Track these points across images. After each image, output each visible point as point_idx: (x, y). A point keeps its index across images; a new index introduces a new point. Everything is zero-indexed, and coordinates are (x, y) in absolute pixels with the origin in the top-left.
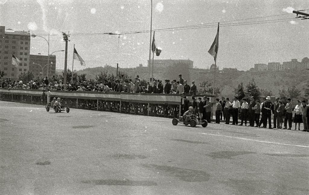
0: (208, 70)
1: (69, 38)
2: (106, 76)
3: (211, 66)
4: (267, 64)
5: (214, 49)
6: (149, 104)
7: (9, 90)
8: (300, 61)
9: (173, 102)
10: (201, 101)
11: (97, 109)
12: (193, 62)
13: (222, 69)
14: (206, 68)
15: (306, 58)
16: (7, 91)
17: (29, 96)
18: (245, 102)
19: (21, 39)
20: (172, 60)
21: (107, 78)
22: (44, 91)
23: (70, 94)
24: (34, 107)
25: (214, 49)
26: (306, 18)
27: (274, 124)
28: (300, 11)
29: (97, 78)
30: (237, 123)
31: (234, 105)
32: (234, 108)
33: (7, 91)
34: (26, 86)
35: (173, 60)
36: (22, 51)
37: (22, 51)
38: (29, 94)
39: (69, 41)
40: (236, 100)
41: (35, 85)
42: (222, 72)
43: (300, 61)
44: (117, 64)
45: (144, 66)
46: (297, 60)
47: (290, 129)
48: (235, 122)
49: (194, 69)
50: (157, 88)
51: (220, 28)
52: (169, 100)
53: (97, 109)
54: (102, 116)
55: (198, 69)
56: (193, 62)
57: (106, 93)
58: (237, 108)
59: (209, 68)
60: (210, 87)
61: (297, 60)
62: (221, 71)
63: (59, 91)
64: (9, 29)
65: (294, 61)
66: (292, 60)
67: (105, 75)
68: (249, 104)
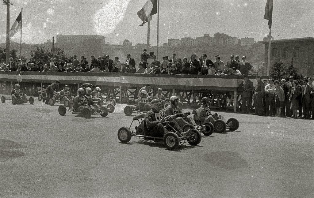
0: (120, 46)
3: (124, 42)
4: (181, 39)
6: (120, 87)
8: (212, 36)
9: (226, 88)
11: (235, 109)
13: (136, 44)
15: (218, 33)
21: (45, 53)
23: (26, 76)
24: (5, 94)
29: (32, 54)
42: (135, 47)
43: (212, 36)
44: (52, 38)
45: (210, 36)
46: (208, 35)
61: (208, 35)
62: (134, 47)
65: (207, 36)
66: (204, 35)
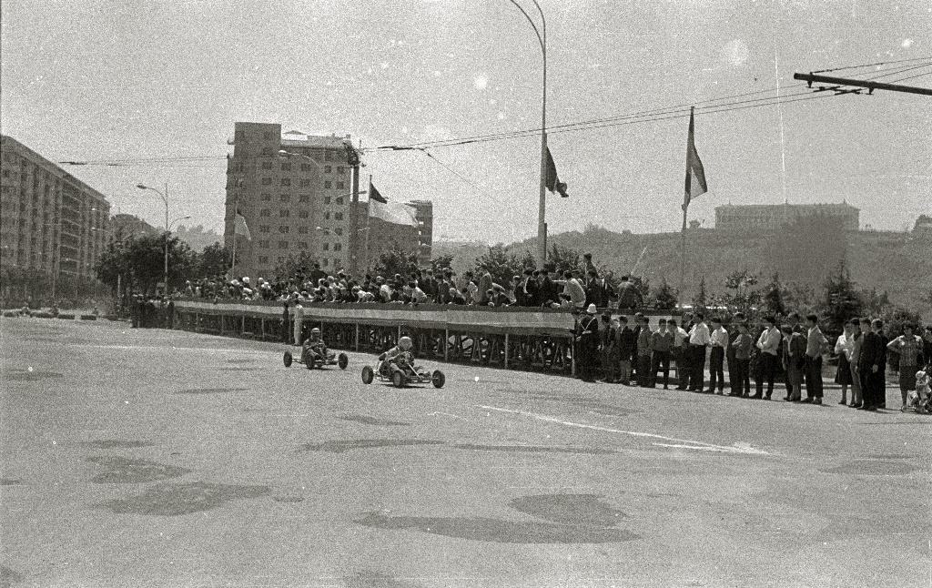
0: (905, 234)
1: (362, 156)
2: (504, 261)
3: (917, 223)
5: (695, 172)
7: (215, 304)
10: (627, 327)
12: (857, 211)
14: (899, 229)
16: (212, 306)
17: (257, 319)
18: (719, 328)
19: (328, 158)
20: (790, 206)
22: (286, 305)
25: (695, 172)
26: (844, 92)
27: (787, 388)
28: (817, 74)
30: (701, 388)
31: (692, 337)
32: (693, 346)
33: (212, 306)
34: (250, 291)
35: (796, 207)
36: (328, 193)
37: (328, 193)
38: (257, 313)
39: (363, 166)
40: (699, 323)
41: (269, 291)
47: (768, 397)
48: (738, 390)
49: (861, 233)
50: (525, 291)
51: (695, 118)
52: (553, 325)
53: (573, 372)
54: (206, 340)
55: (873, 233)
56: (857, 211)
57: (417, 308)
58: (702, 344)
59: (911, 228)
60: (755, 288)
63: (320, 303)
64: (293, 132)
67: (500, 256)
68: (729, 332)
